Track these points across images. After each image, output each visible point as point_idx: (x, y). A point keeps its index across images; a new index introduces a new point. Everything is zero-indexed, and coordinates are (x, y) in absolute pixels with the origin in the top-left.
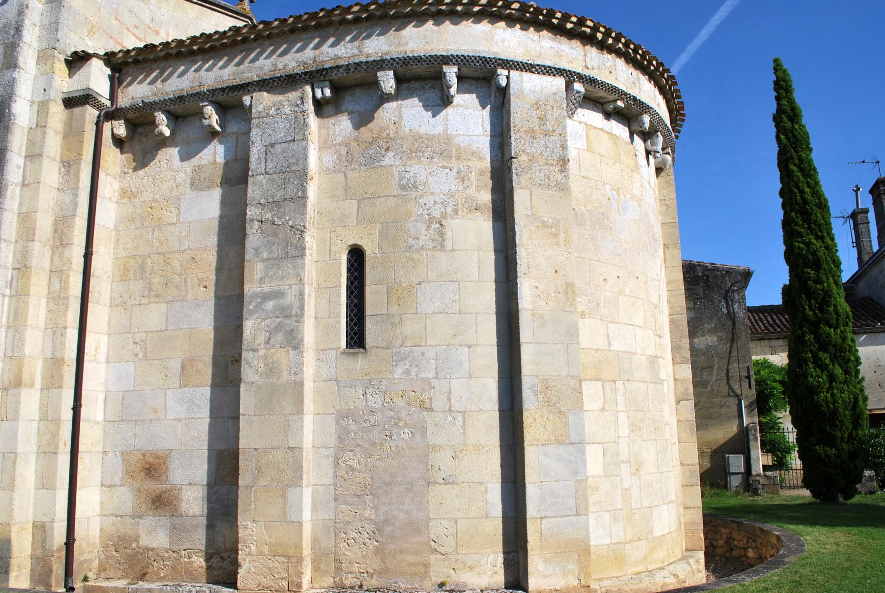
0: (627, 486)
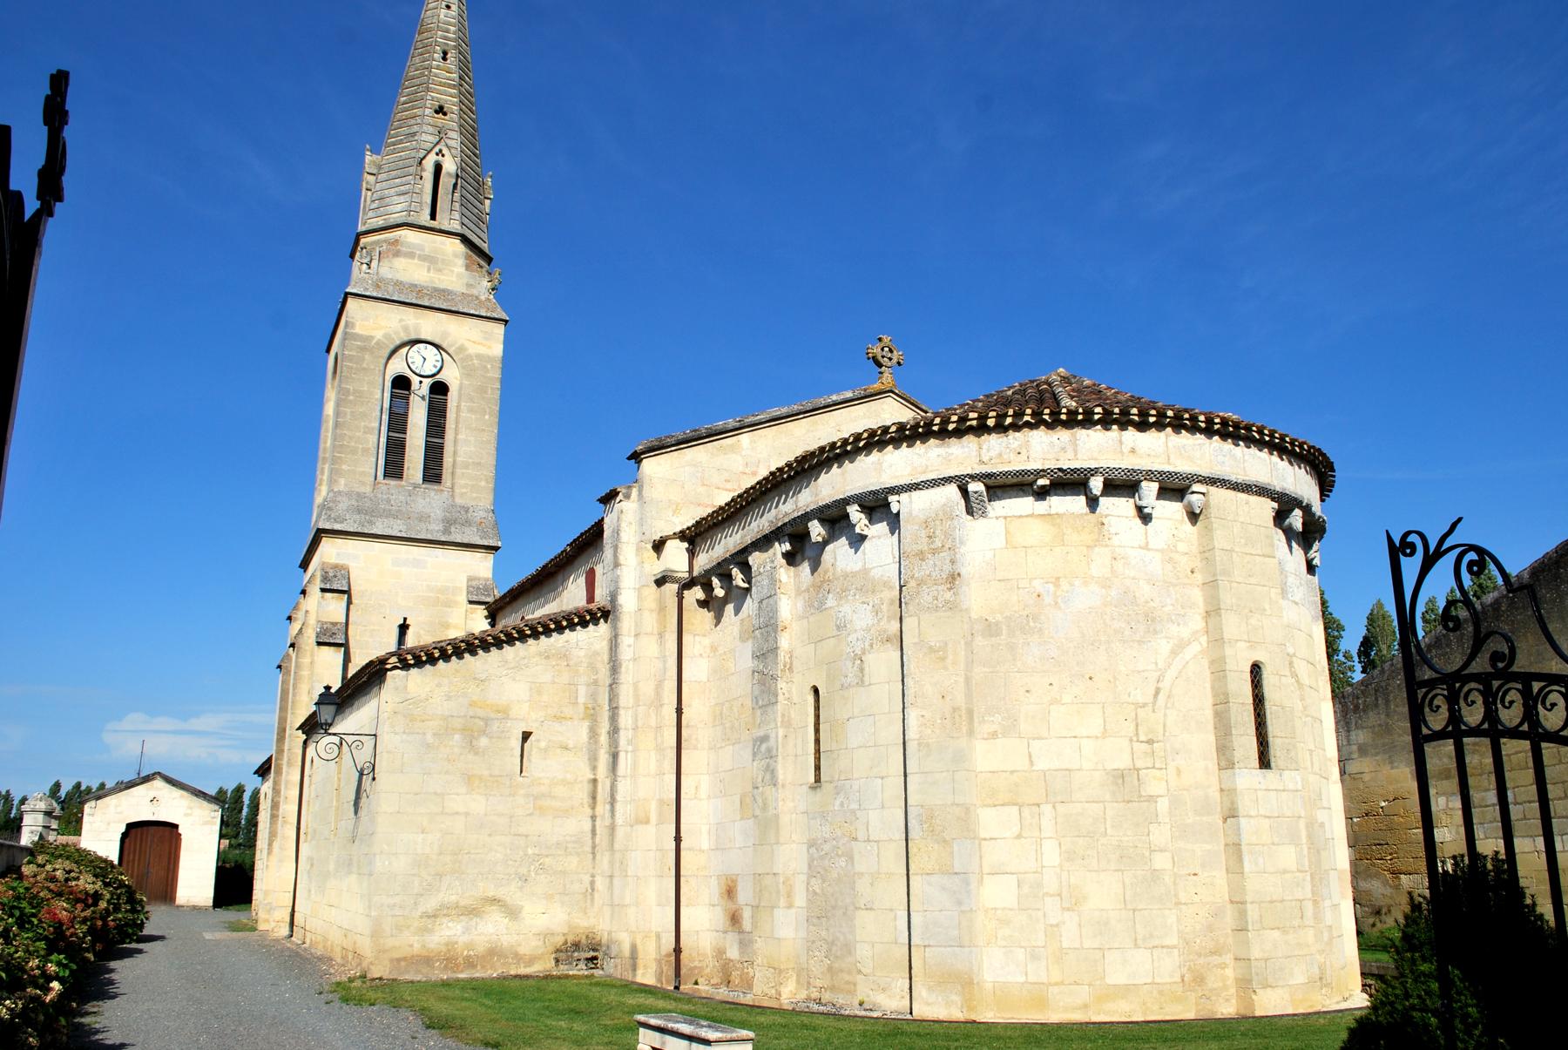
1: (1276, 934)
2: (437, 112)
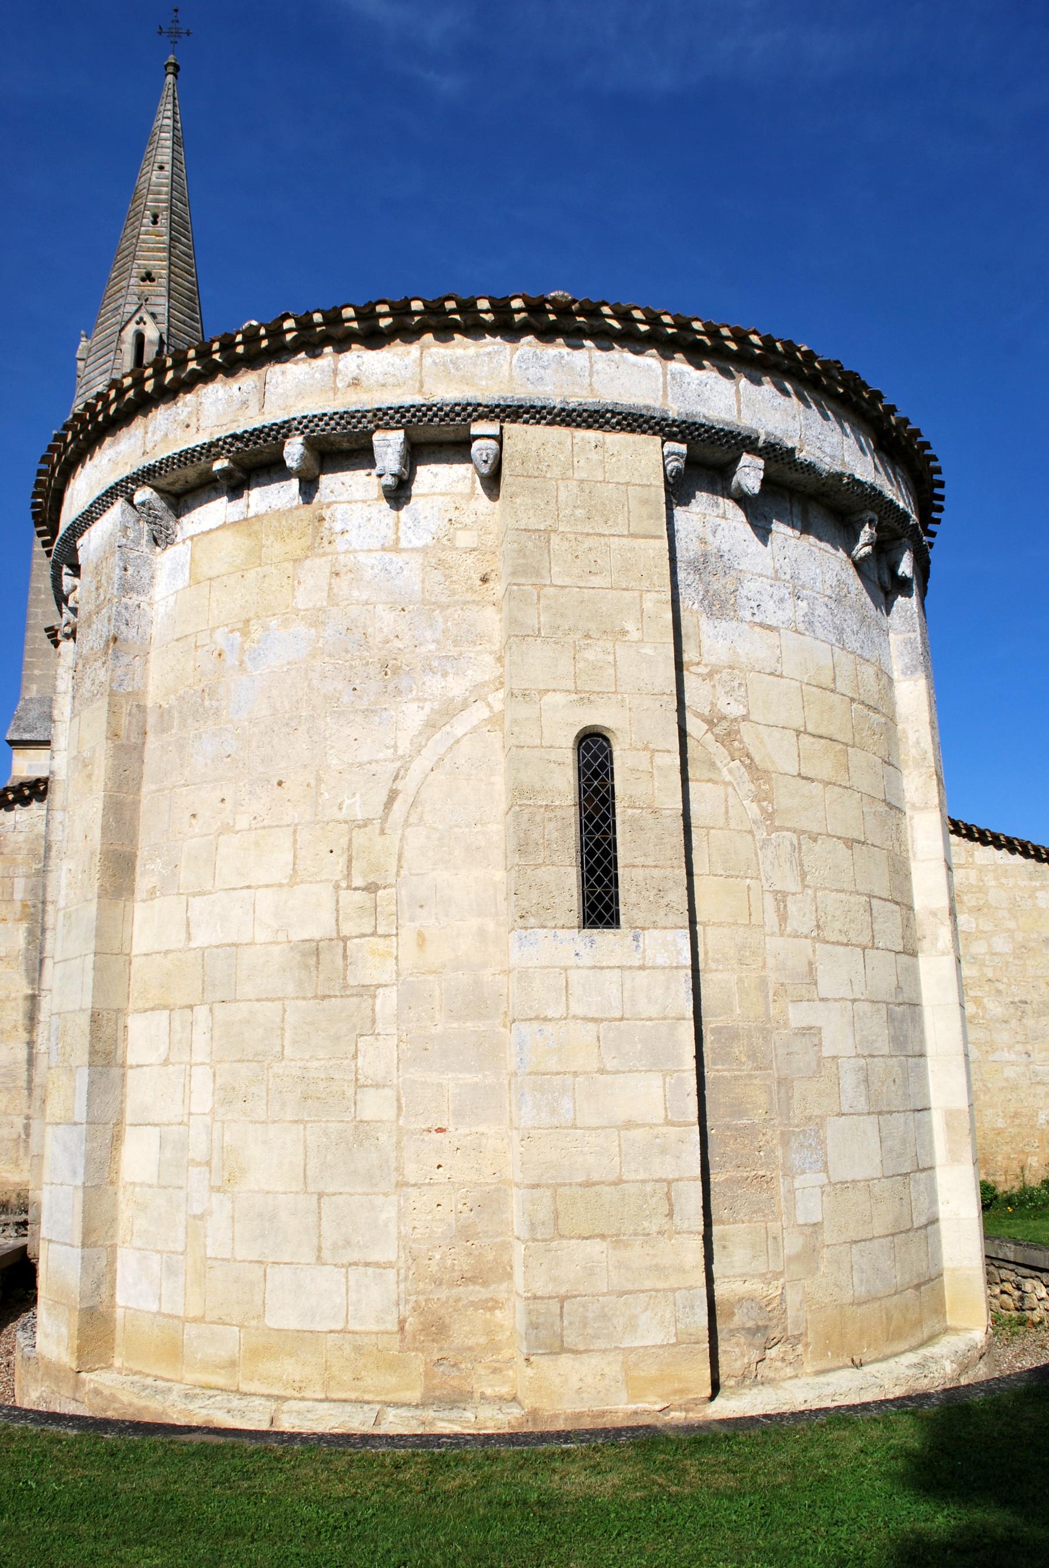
0: (197, 1210)
1: (596, 1247)
2: (143, 280)
